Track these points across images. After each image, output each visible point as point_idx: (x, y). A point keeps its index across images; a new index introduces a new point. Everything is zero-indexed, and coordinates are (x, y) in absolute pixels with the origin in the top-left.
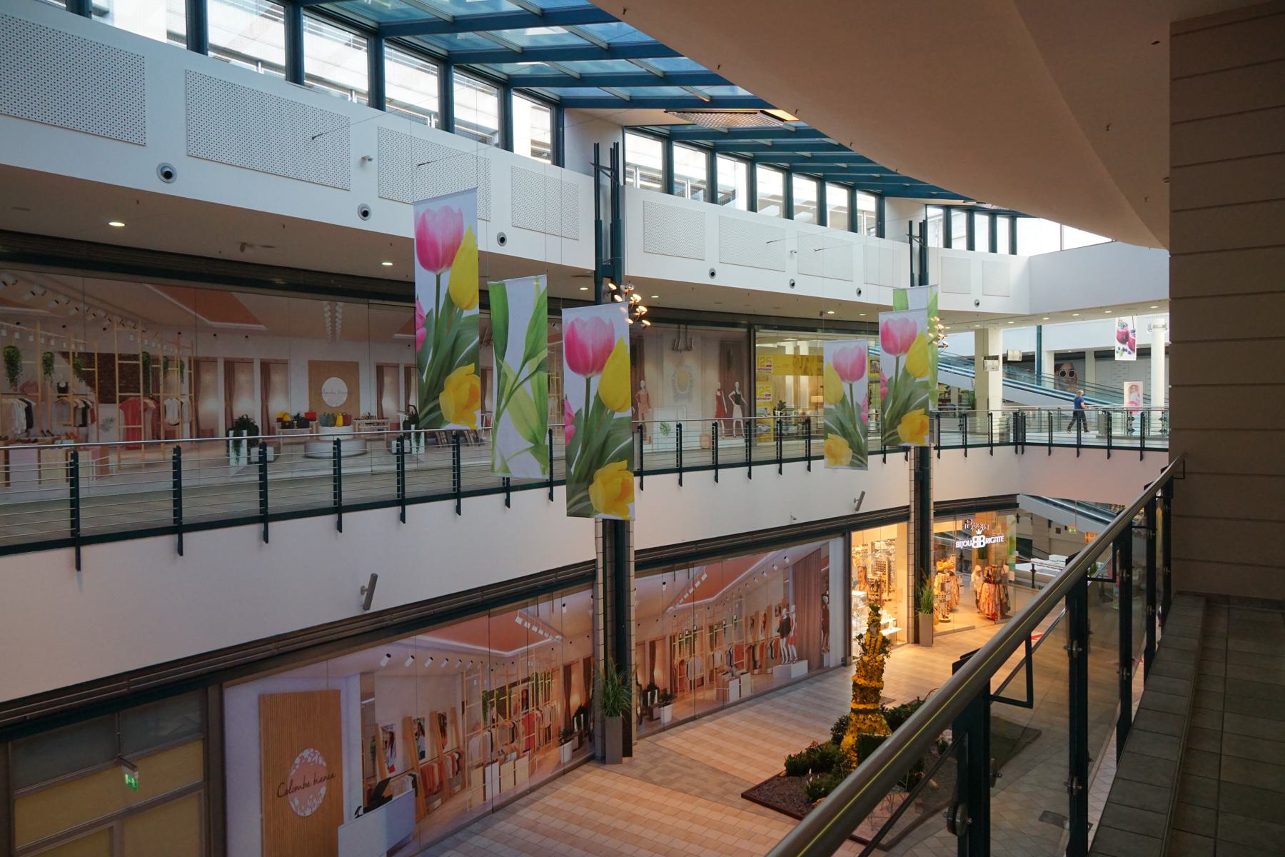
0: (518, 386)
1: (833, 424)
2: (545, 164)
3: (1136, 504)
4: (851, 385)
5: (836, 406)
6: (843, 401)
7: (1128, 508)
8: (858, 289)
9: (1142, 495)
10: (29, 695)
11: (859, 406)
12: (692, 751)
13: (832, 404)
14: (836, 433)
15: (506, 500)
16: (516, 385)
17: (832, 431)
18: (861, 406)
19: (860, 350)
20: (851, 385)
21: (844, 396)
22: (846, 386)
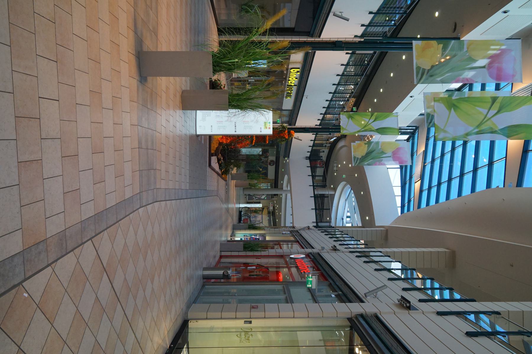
0: (368, 125)
1: (372, 148)
2: (376, 230)
3: (279, 170)
4: (390, 157)
5: (381, 149)
6: (383, 153)
7: (285, 98)
8: (509, 11)
9: (218, 22)
10: (335, 3)
11: (381, 161)
12: (250, 218)
13: (381, 147)
14: (368, 149)
15: (364, 25)
16: (368, 124)
17: (369, 147)
18: (381, 162)
19: (407, 161)
20: (390, 157)
21: (385, 153)
22: (390, 154)
